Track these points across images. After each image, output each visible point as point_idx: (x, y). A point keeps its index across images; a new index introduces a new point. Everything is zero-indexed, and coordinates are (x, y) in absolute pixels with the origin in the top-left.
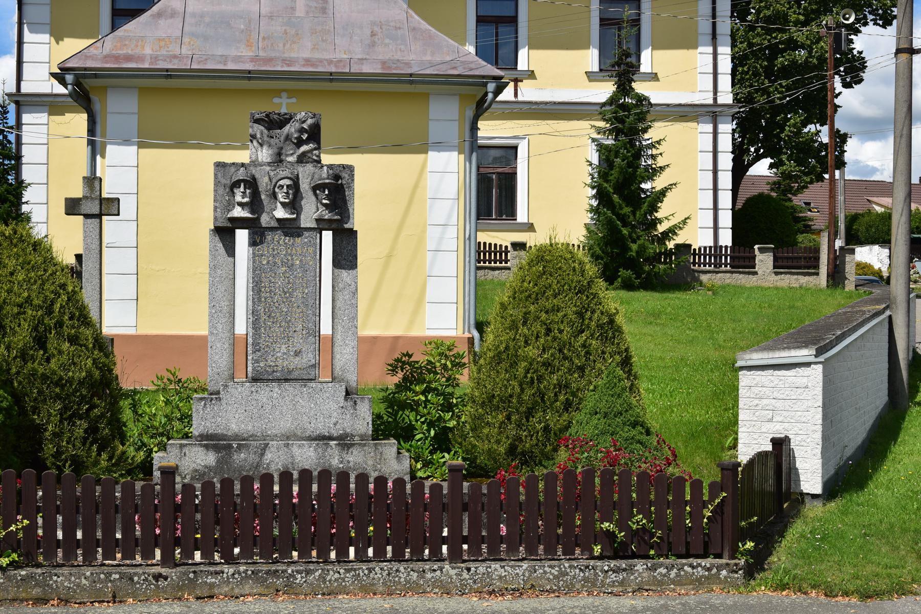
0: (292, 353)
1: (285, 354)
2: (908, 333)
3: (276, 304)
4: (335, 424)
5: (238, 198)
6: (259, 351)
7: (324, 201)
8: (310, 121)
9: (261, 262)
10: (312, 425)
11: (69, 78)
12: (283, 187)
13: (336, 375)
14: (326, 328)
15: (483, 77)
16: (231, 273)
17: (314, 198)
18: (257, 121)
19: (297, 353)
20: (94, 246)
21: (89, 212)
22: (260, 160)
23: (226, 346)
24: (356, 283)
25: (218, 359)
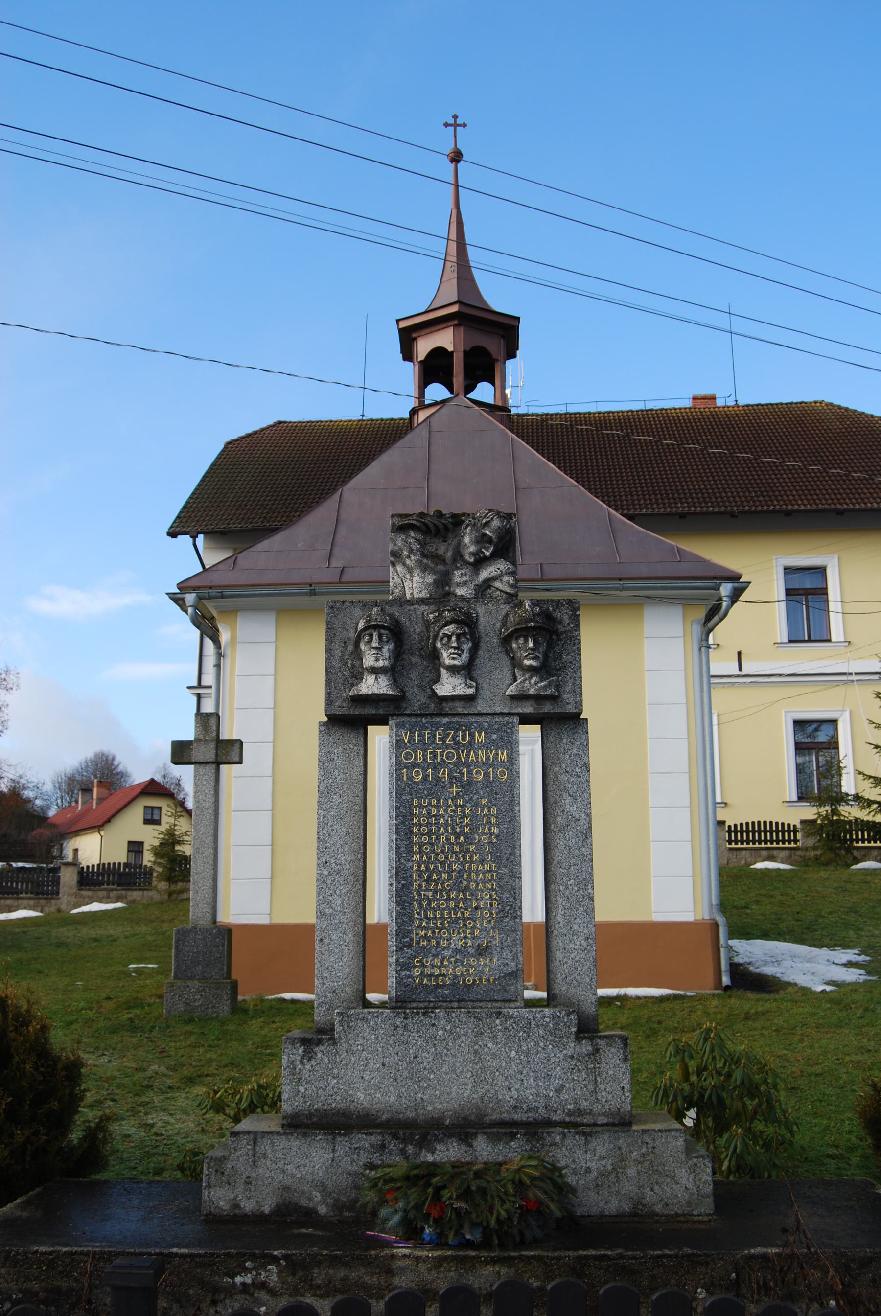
0: (472, 951)
1: (457, 951)
2: (364, 947)
4: (558, 1091)
5: (369, 660)
6: (410, 946)
7: (527, 662)
8: (496, 523)
9: (410, 778)
10: (514, 1093)
11: (190, 598)
12: (449, 637)
13: (556, 991)
14: (533, 910)
15: (715, 578)
16: (359, 801)
17: (505, 661)
18: (402, 529)
19: (482, 951)
21: (201, 759)
22: (408, 596)
23: (349, 938)
24: (589, 815)
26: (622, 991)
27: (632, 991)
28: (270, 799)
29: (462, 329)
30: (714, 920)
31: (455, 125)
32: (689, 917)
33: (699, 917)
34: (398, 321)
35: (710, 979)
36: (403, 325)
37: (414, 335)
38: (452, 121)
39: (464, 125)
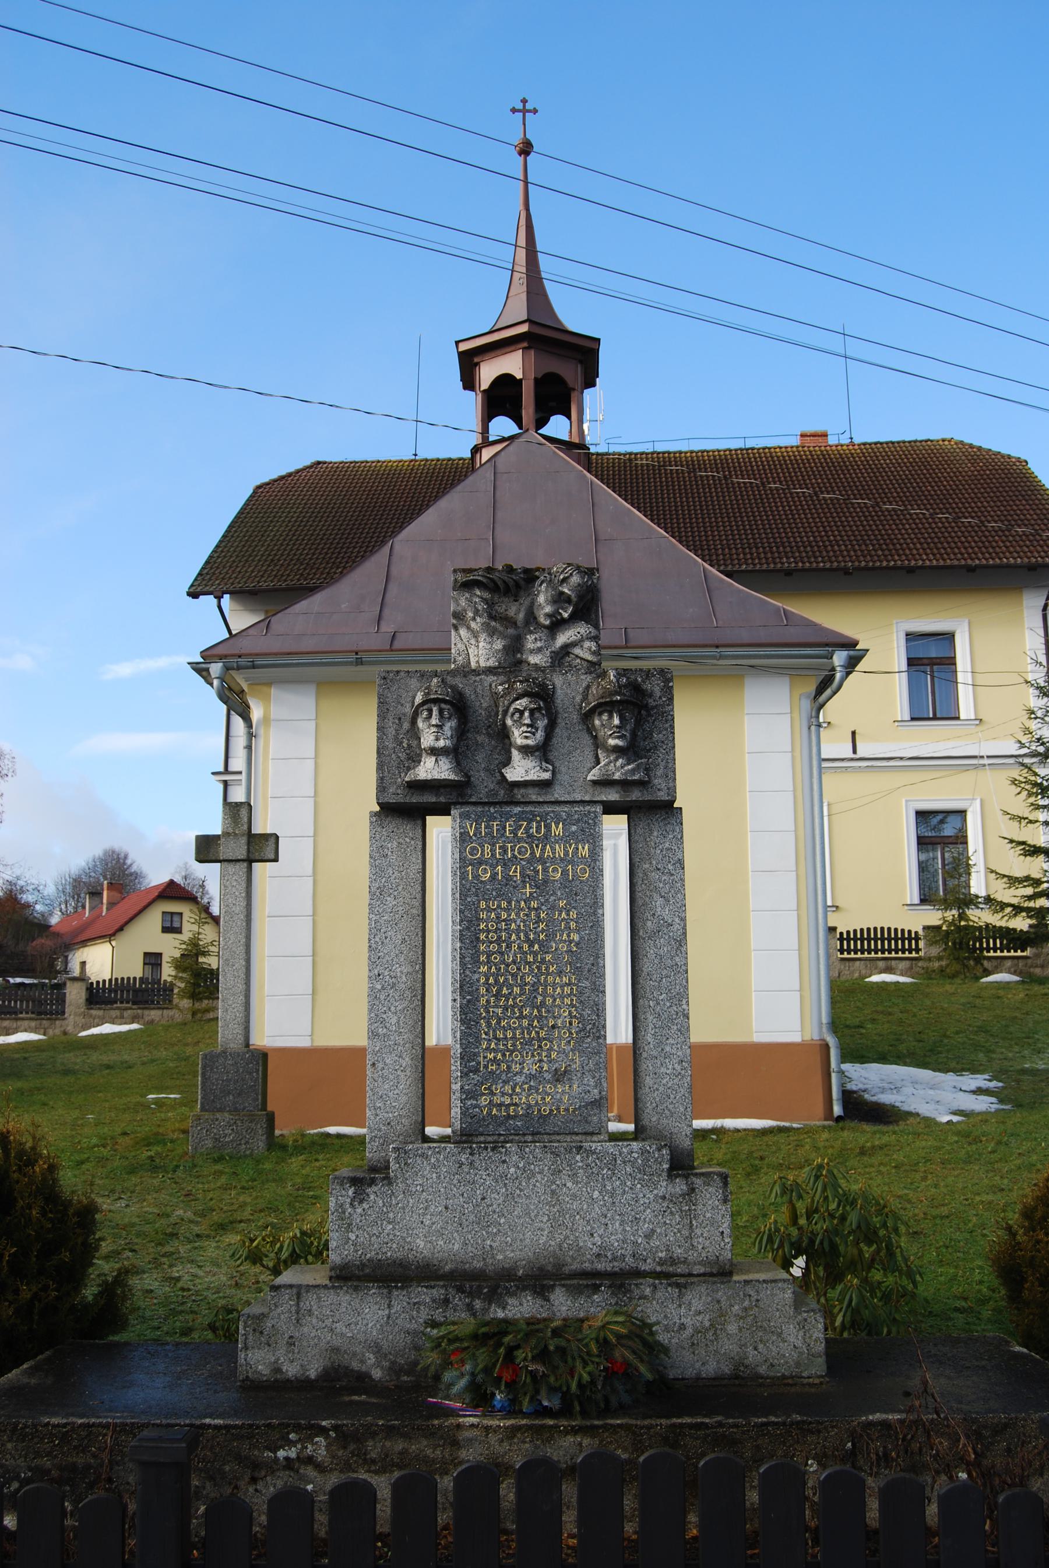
1: (531, 1077)
3: (513, 969)
4: (648, 1236)
5: (428, 739)
6: (476, 1071)
7: (612, 742)
8: (576, 579)
11: (216, 669)
14: (619, 1029)
16: (417, 903)
18: (467, 586)
19: (560, 1076)
20: (237, 909)
22: (473, 665)
23: (407, 1061)
24: (683, 920)
25: (388, 1097)
26: (718, 1123)
27: (730, 1123)
28: (311, 902)
29: (532, 352)
30: (824, 1040)
31: (524, 111)
32: (796, 1038)
33: (807, 1037)
34: (457, 343)
35: (820, 1109)
36: (463, 347)
37: (476, 360)
38: (520, 106)
39: (535, 111)
